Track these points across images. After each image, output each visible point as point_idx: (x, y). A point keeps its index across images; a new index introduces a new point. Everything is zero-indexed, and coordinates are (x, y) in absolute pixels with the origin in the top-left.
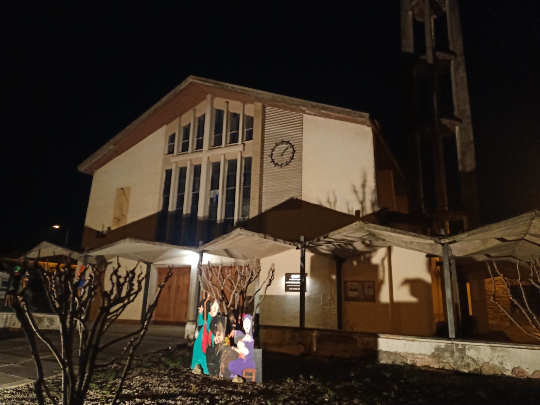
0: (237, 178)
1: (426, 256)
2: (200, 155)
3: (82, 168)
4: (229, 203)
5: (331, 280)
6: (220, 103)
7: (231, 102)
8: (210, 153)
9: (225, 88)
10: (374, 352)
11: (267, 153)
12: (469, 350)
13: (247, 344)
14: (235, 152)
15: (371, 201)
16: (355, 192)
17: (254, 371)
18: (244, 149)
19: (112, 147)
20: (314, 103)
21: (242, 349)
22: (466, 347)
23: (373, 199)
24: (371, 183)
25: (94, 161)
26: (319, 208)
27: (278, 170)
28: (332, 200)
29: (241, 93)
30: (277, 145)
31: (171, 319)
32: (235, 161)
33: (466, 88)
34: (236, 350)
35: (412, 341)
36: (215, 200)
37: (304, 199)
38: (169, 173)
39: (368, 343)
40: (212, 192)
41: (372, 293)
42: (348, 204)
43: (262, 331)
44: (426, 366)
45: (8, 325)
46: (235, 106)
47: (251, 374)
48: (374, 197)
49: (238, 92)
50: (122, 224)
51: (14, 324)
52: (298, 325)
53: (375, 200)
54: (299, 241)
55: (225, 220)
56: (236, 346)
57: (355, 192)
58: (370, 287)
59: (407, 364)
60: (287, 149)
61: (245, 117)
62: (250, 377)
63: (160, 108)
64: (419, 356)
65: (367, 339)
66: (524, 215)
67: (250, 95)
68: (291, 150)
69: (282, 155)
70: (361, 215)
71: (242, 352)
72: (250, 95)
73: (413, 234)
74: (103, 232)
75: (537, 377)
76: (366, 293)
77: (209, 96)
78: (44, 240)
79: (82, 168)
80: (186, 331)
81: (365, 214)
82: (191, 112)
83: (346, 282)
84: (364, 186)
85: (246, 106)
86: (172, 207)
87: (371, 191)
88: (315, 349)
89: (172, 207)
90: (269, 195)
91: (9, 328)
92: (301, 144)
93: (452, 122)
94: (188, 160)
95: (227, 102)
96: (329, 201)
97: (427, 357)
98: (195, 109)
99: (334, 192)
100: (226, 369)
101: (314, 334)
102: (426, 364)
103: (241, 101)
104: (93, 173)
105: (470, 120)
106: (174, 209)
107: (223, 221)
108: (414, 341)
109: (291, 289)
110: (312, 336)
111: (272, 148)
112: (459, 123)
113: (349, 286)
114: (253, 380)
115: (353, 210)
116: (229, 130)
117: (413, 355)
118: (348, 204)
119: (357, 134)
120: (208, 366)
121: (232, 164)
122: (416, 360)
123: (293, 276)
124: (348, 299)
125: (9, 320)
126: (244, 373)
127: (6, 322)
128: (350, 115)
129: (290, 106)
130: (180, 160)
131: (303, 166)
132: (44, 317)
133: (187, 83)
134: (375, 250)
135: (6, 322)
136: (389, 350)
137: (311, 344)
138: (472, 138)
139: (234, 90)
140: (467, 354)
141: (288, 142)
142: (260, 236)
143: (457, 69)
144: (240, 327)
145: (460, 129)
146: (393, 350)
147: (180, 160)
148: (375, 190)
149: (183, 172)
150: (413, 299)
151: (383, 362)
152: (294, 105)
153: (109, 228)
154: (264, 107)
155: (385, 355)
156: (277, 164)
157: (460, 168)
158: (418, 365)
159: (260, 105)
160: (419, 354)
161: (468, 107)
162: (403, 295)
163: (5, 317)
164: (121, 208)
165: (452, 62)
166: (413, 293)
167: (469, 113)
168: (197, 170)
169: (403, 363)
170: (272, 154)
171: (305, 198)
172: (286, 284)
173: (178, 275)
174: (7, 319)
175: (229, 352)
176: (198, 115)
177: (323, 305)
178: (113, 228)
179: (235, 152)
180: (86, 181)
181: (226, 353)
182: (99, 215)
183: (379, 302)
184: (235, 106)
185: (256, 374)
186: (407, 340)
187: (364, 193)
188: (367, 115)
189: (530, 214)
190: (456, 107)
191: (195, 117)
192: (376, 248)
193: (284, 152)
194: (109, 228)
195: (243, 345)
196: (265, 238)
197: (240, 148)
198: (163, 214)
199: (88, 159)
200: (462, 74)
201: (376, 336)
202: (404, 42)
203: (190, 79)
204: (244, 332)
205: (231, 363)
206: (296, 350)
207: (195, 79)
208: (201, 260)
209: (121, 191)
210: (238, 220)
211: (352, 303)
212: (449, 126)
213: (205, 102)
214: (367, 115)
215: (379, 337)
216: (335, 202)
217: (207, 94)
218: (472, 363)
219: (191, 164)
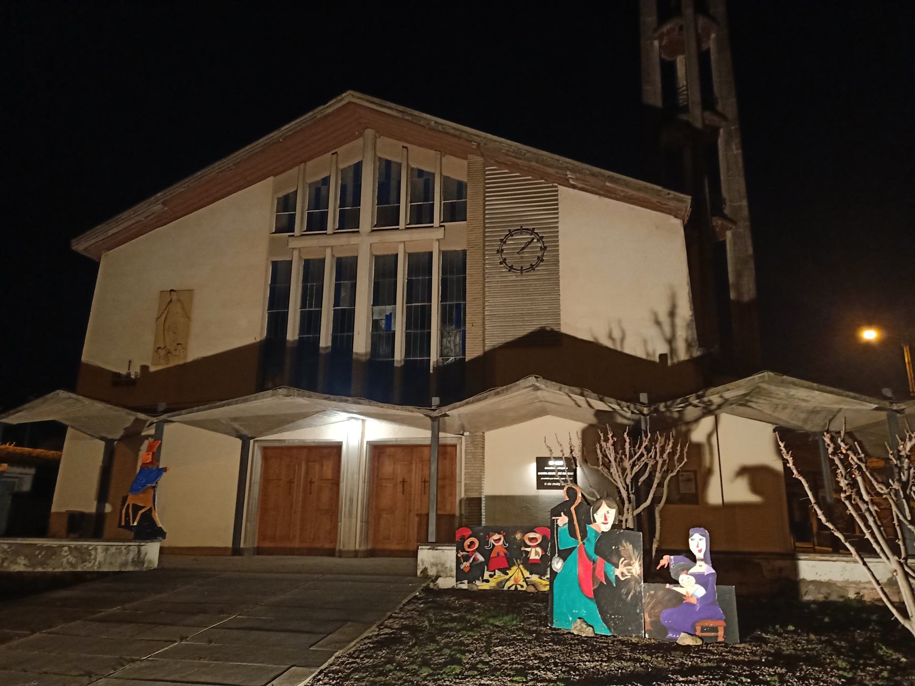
1: (774, 431)
2: (354, 240)
3: (80, 245)
8: (376, 238)
10: (793, 583)
13: (700, 579)
14: (432, 239)
15: (687, 340)
16: (658, 323)
24: (685, 311)
26: (592, 348)
27: (514, 278)
28: (617, 334)
30: (511, 234)
31: (296, 544)
33: (742, 173)
36: (383, 324)
37: (564, 329)
39: (781, 570)
40: (376, 308)
41: (693, 491)
42: (645, 342)
46: (422, 158)
47: (715, 629)
48: (690, 333)
49: (448, 133)
54: (636, 400)
55: (406, 361)
56: (676, 583)
57: (658, 323)
58: (689, 480)
60: (530, 243)
65: (780, 563)
70: (669, 362)
71: (691, 593)
73: (852, 394)
74: (129, 375)
76: (682, 491)
77: (369, 132)
79: (80, 245)
80: (419, 562)
81: (675, 360)
84: (672, 314)
85: (444, 159)
87: (685, 324)
89: (292, 333)
90: (492, 323)
96: (610, 337)
99: (619, 322)
100: (656, 623)
105: (747, 223)
106: (297, 338)
109: (549, 484)
117: (857, 583)
118: (645, 342)
119: (657, 228)
121: (420, 264)
123: (551, 463)
126: (698, 628)
136: (817, 578)
138: (750, 251)
139: (440, 128)
143: (728, 143)
145: (733, 235)
146: (824, 578)
147: (303, 246)
149: (313, 270)
150: (754, 498)
152: (551, 166)
157: (732, 296)
158: (867, 598)
161: (744, 203)
162: (740, 492)
165: (722, 131)
166: (755, 488)
167: (745, 212)
168: (346, 269)
169: (842, 597)
172: (538, 477)
173: (308, 461)
175: (660, 593)
178: (152, 369)
179: (432, 239)
180: (88, 269)
183: (706, 504)
184: (422, 158)
185: (726, 630)
194: (144, 368)
195: (693, 580)
200: (735, 152)
201: (792, 558)
202: (647, 88)
203: (349, 96)
204: (693, 559)
207: (359, 98)
213: (360, 141)
216: (623, 339)
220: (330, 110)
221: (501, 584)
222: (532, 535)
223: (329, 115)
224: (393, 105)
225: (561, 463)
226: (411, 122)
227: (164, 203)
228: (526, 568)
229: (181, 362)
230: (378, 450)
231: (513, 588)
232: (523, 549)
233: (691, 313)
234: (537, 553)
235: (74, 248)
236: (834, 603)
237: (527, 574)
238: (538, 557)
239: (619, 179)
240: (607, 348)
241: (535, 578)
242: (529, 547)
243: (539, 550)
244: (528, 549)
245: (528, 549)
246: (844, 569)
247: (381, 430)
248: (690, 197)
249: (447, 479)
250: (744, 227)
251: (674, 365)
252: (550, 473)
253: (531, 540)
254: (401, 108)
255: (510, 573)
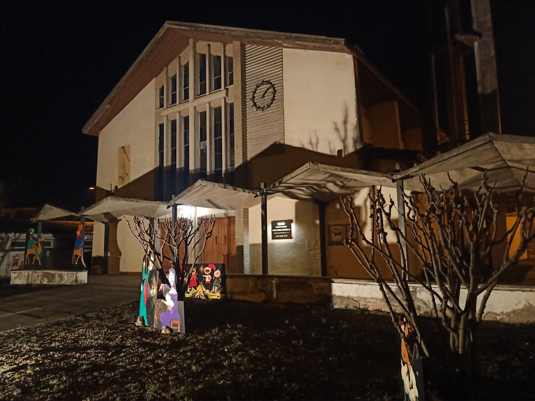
0: (220, 126)
2: (187, 105)
3: (86, 131)
4: (217, 154)
5: (315, 225)
6: (202, 47)
7: (213, 44)
8: (195, 103)
9: (199, 29)
10: (328, 297)
11: (249, 96)
12: (420, 292)
13: (172, 296)
14: (217, 98)
15: (353, 138)
16: (337, 130)
17: (178, 322)
18: (227, 95)
19: (108, 106)
20: (288, 34)
21: (169, 302)
22: (417, 290)
23: (355, 137)
24: (353, 119)
25: (95, 122)
27: (261, 114)
28: (314, 141)
29: (217, 33)
32: (220, 108)
34: (165, 302)
35: (364, 284)
37: (287, 142)
38: (161, 126)
39: (323, 289)
40: (202, 143)
42: (330, 144)
43: (228, 280)
44: (378, 310)
45: (30, 281)
46: (217, 49)
48: (356, 132)
50: (127, 182)
51: (35, 281)
52: (260, 273)
53: (357, 137)
54: (259, 189)
55: (215, 171)
57: (337, 130)
59: (359, 308)
60: (268, 89)
61: (227, 59)
62: (176, 328)
63: (143, 60)
64: (371, 300)
66: (476, 140)
67: (224, 34)
68: (271, 90)
69: (264, 97)
70: (343, 155)
72: (224, 34)
73: (364, 171)
75: (490, 319)
78: (46, 202)
79: (86, 131)
81: (347, 153)
82: (176, 60)
83: (329, 226)
84: (345, 122)
86: (167, 162)
87: (353, 127)
88: (275, 296)
89: (167, 162)
91: (31, 284)
92: (282, 82)
93: (469, 37)
94: (176, 112)
95: (209, 45)
96: (311, 143)
97: (378, 301)
98: (180, 57)
101: (274, 282)
102: (378, 308)
103: (221, 42)
104: (98, 134)
105: (491, 32)
107: (213, 172)
108: (366, 285)
109: (278, 236)
110: (272, 283)
111: (253, 90)
112: (478, 38)
113: (333, 230)
114: (179, 331)
115: (335, 150)
116: (213, 75)
117: (365, 299)
118: (330, 144)
119: (337, 64)
120: (147, 317)
121: (218, 111)
122: (368, 304)
123: (279, 224)
124: (332, 243)
125: (30, 277)
127: (28, 279)
128: (325, 43)
129: (264, 40)
130: (173, 112)
131: (284, 106)
132: (56, 273)
133: (165, 29)
134: (358, 191)
135: (28, 279)
136: (342, 294)
137: (271, 291)
138: (493, 53)
140: (417, 297)
141: (268, 82)
142: (220, 186)
144: (166, 282)
145: (479, 44)
146: (346, 295)
147: (173, 112)
148: (357, 125)
151: (336, 307)
153: (116, 187)
154: (243, 46)
155: (338, 300)
156: (259, 108)
157: (479, 90)
158: (370, 309)
159: (238, 43)
160: (371, 298)
161: (489, 16)
163: (26, 274)
164: (124, 168)
167: (489, 24)
169: (355, 307)
170: (254, 97)
171: (288, 142)
172: (273, 232)
174: (28, 276)
175: (160, 305)
176: (183, 63)
177: (308, 251)
178: (119, 187)
180: (92, 143)
181: (158, 305)
182: (107, 177)
186: (359, 284)
187: (346, 130)
188: (342, 40)
189: (483, 138)
190: (475, 20)
191: (180, 65)
192: (358, 189)
193: (266, 92)
194: (116, 187)
196: (225, 188)
197: (223, 94)
198: (159, 171)
199: (90, 121)
203: (167, 25)
205: (162, 315)
206: (257, 298)
207: (171, 24)
208: (196, 213)
209: (123, 149)
210: (226, 170)
211: (336, 247)
212: (466, 43)
213: (187, 49)
214: (342, 40)
215: (334, 282)
217: (188, 39)
218: (422, 306)
219: (181, 117)
220: (160, 35)
221: (194, 294)
222: (207, 268)
223: (161, 38)
224: (185, 23)
225: (283, 224)
226: (194, 30)
227: (110, 103)
228: (204, 286)
229: (128, 183)
230: (203, 221)
231: (198, 297)
232: (203, 276)
233: (356, 119)
234: (209, 278)
235: (83, 132)
236: (351, 310)
237: (204, 290)
238: (209, 281)
239: (301, 37)
240: (309, 151)
241: (207, 291)
242: (206, 275)
243: (210, 276)
244: (205, 276)
245: (205, 276)
246: (358, 289)
247: (205, 212)
248: (343, 39)
249: (230, 238)
250: (488, 36)
251: (346, 156)
252: (278, 230)
253: (207, 271)
254: (189, 24)
255: (198, 288)
